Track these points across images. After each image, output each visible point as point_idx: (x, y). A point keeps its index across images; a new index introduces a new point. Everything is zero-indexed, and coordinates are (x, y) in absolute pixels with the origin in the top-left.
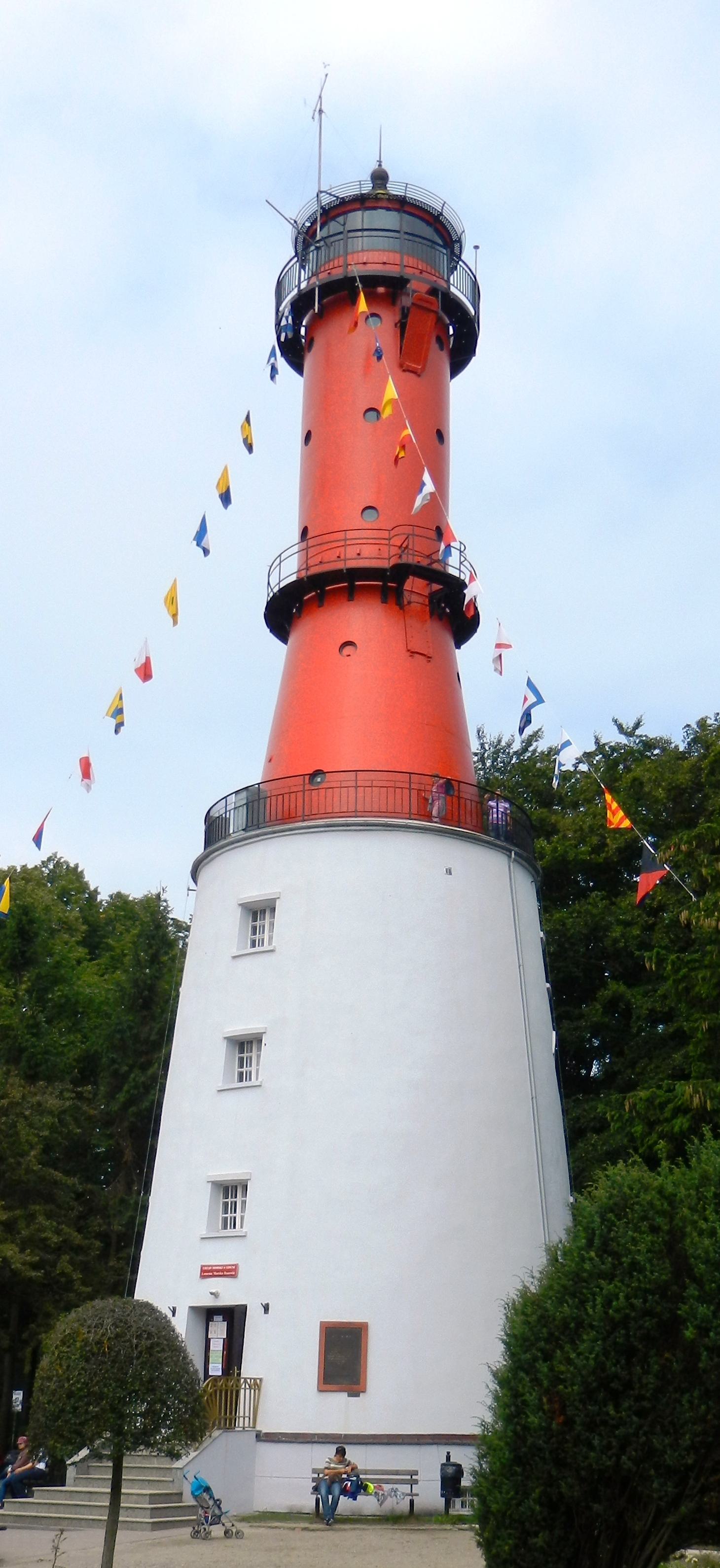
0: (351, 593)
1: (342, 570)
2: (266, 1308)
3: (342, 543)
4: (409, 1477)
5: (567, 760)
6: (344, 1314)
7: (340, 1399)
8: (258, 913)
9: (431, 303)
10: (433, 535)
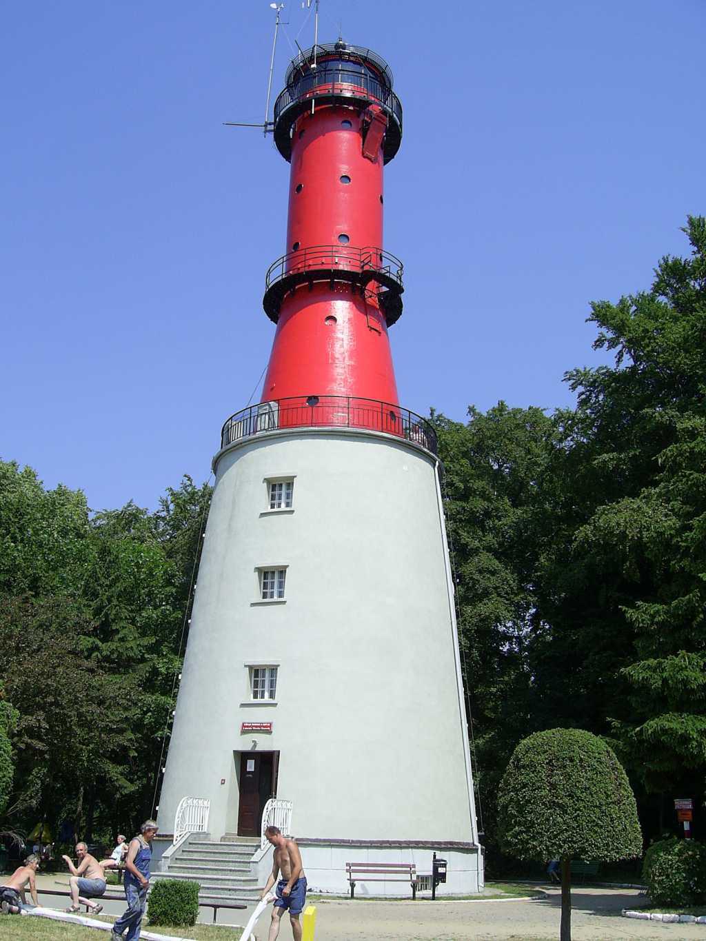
4: (409, 869)
8: (280, 488)
9: (383, 120)
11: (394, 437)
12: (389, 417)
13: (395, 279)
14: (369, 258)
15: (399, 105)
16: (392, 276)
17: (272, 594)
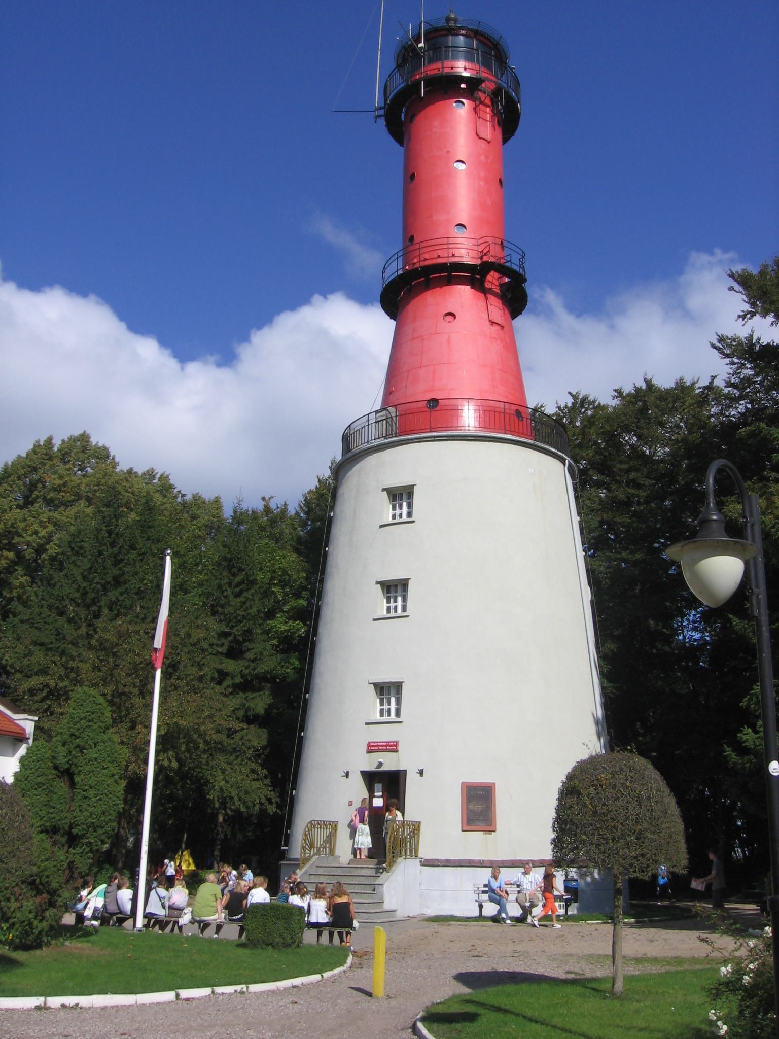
0: (451, 281)
1: (446, 264)
2: (421, 773)
3: (446, 246)
5: (292, 511)
6: (479, 777)
7: (477, 837)
8: (401, 495)
10: (505, 244)
11: (529, 441)
12: (517, 420)
13: (517, 269)
14: (487, 249)
15: (517, 82)
16: (514, 267)
17: (396, 608)
